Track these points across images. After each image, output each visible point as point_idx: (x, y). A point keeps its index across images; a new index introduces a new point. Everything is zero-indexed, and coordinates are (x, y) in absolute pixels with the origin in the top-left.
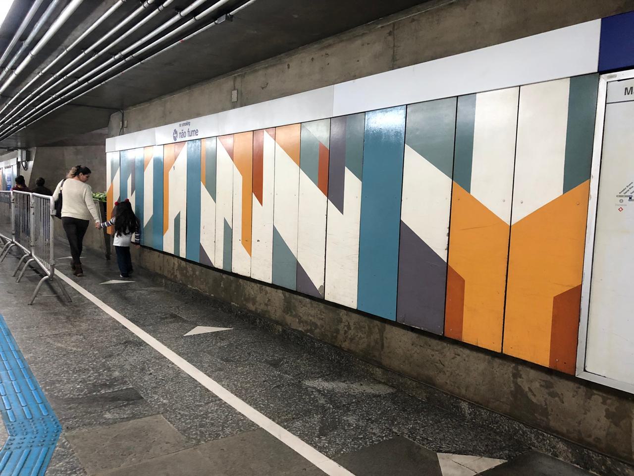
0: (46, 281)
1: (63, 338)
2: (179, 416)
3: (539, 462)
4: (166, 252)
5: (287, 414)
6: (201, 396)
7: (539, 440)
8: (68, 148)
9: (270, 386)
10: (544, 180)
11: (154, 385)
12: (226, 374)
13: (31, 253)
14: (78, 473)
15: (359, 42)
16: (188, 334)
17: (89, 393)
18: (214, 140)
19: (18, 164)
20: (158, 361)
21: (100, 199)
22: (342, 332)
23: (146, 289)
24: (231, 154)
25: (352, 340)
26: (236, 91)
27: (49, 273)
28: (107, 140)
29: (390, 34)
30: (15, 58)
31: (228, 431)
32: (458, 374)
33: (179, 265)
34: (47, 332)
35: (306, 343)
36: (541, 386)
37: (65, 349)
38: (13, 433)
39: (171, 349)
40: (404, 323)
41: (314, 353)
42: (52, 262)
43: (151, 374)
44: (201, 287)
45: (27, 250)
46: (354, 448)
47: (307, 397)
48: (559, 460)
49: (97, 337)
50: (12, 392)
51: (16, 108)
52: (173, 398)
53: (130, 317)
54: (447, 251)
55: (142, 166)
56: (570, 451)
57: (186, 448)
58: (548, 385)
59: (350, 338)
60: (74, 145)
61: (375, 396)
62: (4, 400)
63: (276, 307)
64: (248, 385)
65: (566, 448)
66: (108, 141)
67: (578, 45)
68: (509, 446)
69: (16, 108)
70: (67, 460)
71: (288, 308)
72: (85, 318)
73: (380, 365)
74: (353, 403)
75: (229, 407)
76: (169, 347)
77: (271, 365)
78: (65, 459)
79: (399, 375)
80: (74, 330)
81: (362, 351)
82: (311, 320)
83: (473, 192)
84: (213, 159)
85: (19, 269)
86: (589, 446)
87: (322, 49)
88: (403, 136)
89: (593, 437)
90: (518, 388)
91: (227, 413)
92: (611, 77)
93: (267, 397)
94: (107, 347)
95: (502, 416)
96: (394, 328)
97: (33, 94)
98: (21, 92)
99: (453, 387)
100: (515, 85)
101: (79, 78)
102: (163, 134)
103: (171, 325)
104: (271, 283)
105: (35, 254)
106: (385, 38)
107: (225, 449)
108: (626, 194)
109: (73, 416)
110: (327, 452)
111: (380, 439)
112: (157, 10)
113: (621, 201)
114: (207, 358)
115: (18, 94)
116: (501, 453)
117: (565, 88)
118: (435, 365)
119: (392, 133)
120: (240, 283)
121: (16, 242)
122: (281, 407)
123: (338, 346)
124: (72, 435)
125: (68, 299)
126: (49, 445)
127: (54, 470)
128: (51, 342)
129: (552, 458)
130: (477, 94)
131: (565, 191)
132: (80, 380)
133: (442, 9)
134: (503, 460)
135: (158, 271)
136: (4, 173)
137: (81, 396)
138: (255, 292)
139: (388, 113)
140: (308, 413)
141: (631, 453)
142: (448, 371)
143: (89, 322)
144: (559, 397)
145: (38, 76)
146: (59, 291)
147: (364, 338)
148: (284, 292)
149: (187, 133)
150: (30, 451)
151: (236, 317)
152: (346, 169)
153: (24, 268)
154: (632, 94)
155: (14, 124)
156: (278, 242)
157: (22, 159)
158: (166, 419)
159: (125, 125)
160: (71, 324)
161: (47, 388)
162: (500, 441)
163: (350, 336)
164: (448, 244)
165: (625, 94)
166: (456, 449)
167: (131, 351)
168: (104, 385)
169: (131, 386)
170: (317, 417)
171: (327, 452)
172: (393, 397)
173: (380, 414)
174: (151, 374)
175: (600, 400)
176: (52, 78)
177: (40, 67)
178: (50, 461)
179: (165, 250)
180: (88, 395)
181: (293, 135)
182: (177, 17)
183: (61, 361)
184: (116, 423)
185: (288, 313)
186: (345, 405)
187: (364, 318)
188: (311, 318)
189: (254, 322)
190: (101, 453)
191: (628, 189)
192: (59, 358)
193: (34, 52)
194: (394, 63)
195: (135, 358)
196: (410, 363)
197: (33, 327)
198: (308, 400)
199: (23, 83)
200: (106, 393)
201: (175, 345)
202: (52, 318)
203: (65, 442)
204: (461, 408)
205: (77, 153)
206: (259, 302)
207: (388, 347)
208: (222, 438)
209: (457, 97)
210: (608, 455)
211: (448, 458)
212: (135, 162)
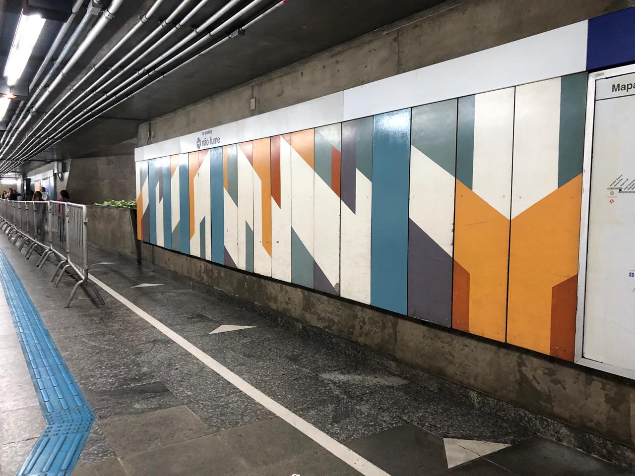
0: (81, 285)
1: (97, 338)
2: (202, 407)
3: (543, 447)
4: (193, 256)
5: (303, 404)
6: (223, 388)
7: (544, 426)
8: (101, 158)
9: (288, 380)
10: (539, 177)
11: (180, 379)
12: (247, 368)
13: (67, 260)
14: (109, 455)
15: (366, 48)
16: (210, 333)
17: (120, 386)
18: (235, 146)
19: (55, 175)
20: (183, 357)
21: (131, 206)
22: (358, 328)
23: (175, 291)
24: (251, 159)
25: (367, 334)
26: (254, 100)
27: (83, 277)
28: (135, 149)
29: (395, 40)
30: (48, 77)
31: (246, 419)
32: (467, 365)
33: (206, 267)
34: (83, 332)
35: (325, 339)
36: (545, 374)
37: (99, 347)
38: (51, 421)
39: (196, 346)
40: (414, 317)
41: (333, 348)
42: (86, 267)
43: (177, 369)
44: (227, 288)
45: (63, 257)
46: (364, 434)
47: (323, 389)
48: (563, 444)
49: (127, 336)
50: (50, 386)
51: (51, 122)
52: (197, 390)
53: (159, 317)
54: (452, 246)
55: (169, 174)
56: (572, 435)
57: (206, 434)
58: (550, 373)
59: (365, 333)
60: (107, 155)
61: (389, 387)
62: (43, 393)
63: (296, 305)
64: (268, 378)
65: (569, 433)
66: (136, 150)
67: (569, 44)
68: (515, 432)
69: (51, 122)
70: (99, 444)
71: (308, 306)
72: (117, 319)
73: (395, 359)
74: (367, 393)
75: (249, 398)
76: (194, 344)
77: (291, 359)
78: (98, 443)
79: (412, 367)
80: (107, 330)
81: (376, 345)
82: (328, 317)
83: (476, 189)
84: (234, 165)
85: (57, 275)
86: (591, 430)
87: (333, 56)
88: (409, 137)
89: (595, 422)
90: (523, 377)
91: (247, 404)
92: (599, 75)
93: (285, 389)
94: (136, 345)
95: (508, 403)
96: (406, 322)
97: (65, 109)
98: (54, 108)
99: (462, 377)
100: (557, 76)
101: (198, 26)
102: (187, 143)
103: (198, 325)
104: (370, 304)
105: (71, 261)
106: (391, 44)
107: (243, 435)
108: (617, 187)
109: (106, 406)
110: (338, 438)
111: (390, 426)
112: (175, 28)
113: (612, 193)
114: (231, 354)
115: (52, 110)
116: (506, 438)
117: (556, 88)
118: (446, 357)
119: (399, 135)
120: (262, 283)
121: (54, 250)
122: (298, 398)
123: (355, 341)
124: (104, 422)
125: (101, 302)
126: (83, 431)
127: (88, 454)
128: (86, 341)
129: (556, 443)
130: (476, 95)
131: (560, 186)
132: (111, 375)
133: (442, 15)
134: (507, 445)
135: (186, 274)
136: (41, 184)
137: (113, 389)
138: (277, 292)
139: (395, 115)
140: (323, 402)
141: (630, 436)
142: (457, 362)
143: (120, 323)
144: (562, 384)
145: (69, 93)
146: (93, 295)
147: (378, 332)
148: (303, 290)
149: (209, 141)
150: (66, 437)
151: (259, 316)
152: (357, 171)
153: (61, 273)
154: (619, 90)
155: (50, 137)
156: (296, 244)
157: (58, 171)
158: (190, 408)
159: (152, 135)
160: (105, 325)
161: (82, 382)
162: (507, 428)
163: (365, 331)
164: (453, 240)
165: (613, 91)
166: (462, 435)
167: (159, 348)
168: (133, 380)
169: (158, 380)
170: (331, 407)
171: (338, 438)
172: (405, 389)
173: (392, 404)
174: (177, 369)
175: (600, 385)
176: (83, 94)
177: (71, 84)
178: (84, 445)
179: (192, 254)
180: (119, 388)
181: (306, 141)
182: (193, 34)
183: (95, 358)
184: (143, 412)
185: (307, 311)
186: (358, 396)
187: (377, 314)
188: (328, 315)
189: (276, 320)
190: (130, 438)
191: (618, 181)
192: (93, 355)
193: (20, 129)
194: (400, 69)
195: (162, 355)
196: (422, 355)
197: (70, 328)
198: (323, 391)
199: (57, 99)
200: (135, 386)
201: (201, 342)
202: (86, 319)
203: (98, 429)
204: (471, 398)
205: (109, 163)
206: (280, 301)
207: (401, 340)
208: (241, 425)
209: (458, 98)
210: (609, 439)
211: (454, 443)
212: (162, 170)
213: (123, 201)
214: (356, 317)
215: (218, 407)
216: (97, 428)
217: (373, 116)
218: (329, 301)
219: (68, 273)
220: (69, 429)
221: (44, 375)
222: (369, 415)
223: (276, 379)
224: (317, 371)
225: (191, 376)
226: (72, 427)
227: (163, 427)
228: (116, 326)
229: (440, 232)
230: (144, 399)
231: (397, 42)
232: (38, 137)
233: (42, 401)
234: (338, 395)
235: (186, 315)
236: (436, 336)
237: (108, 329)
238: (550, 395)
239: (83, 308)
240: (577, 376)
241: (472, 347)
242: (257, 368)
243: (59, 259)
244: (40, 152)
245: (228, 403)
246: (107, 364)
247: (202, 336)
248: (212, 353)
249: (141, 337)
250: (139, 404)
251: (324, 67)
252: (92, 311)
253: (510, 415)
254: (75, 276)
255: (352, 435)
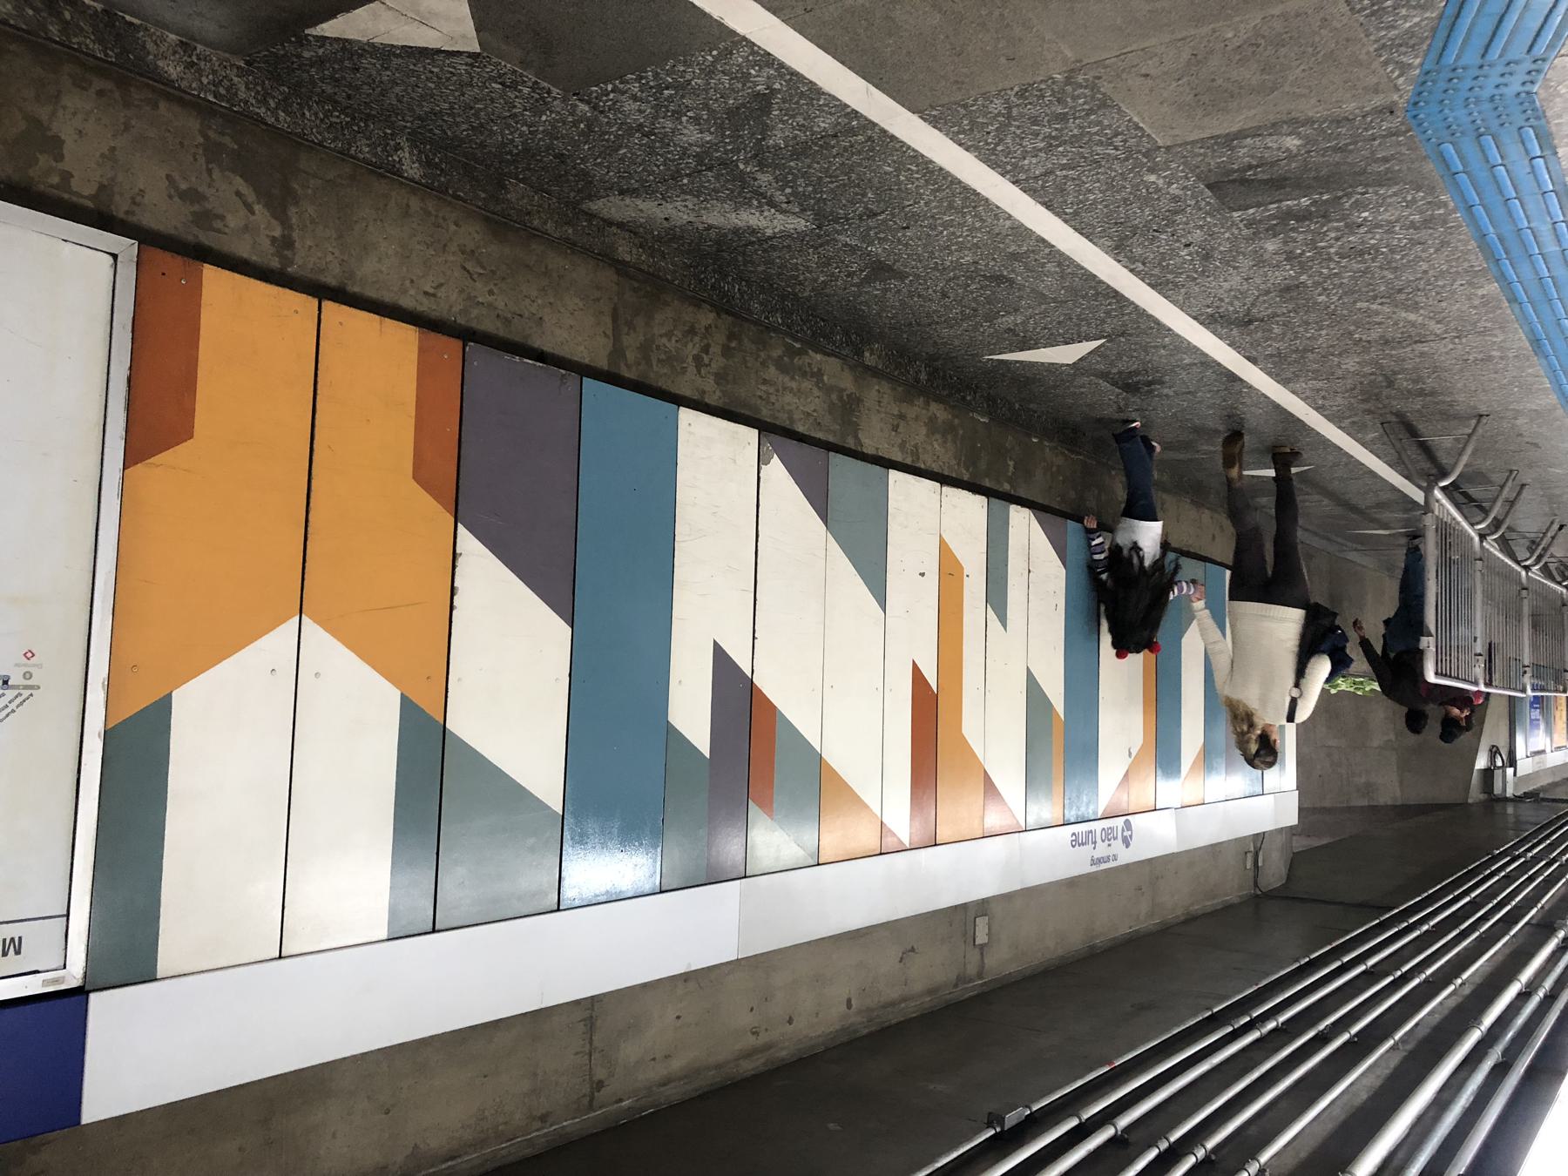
0: (1444, 474)
6: (1062, 190)
10: (222, 729)
15: (677, 1064)
18: (1031, 822)
19: (1512, 762)
20: (1170, 276)
22: (715, 349)
24: (990, 788)
25: (692, 331)
26: (978, 942)
28: (1295, 822)
29: (600, 1085)
30: (1520, 1021)
31: (997, 106)
34: (1442, 348)
36: (222, 218)
41: (783, 298)
42: (1429, 521)
53: (1237, 386)
58: (205, 218)
59: (695, 334)
60: (1374, 809)
61: (633, 192)
65: (160, 63)
67: (135, 1061)
70: (1394, 33)
71: (848, 408)
73: (620, 267)
77: (890, 269)
79: (575, 244)
82: (793, 378)
87: (768, 1047)
90: (279, 212)
95: (320, 144)
96: (587, 361)
98: (1507, 938)
102: (1158, 835)
106: (611, 1075)
107: (1003, 60)
108: (16, 692)
112: (1172, 1139)
113: (28, 675)
114: (1048, 284)
116: (321, 51)
117: (168, 956)
118: (483, 267)
122: (865, 163)
123: (724, 316)
128: (1432, 325)
132: (1362, 230)
137: (1360, 189)
140: (800, 151)
145: (1465, 976)
150: (1483, 56)
156: (873, 569)
160: (1381, 367)
162: (322, 80)
163: (697, 339)
164: (454, 567)
168: (1303, 216)
169: (1235, 214)
170: (777, 138)
171: (753, 53)
172: (589, 188)
173: (620, 147)
175: (75, 184)
176: (1429, 972)
178: (1434, 30)
181: (837, 834)
182: (1124, 1121)
183: (1408, 276)
184: (1274, 125)
187: (664, 384)
188: (794, 385)
191: (13, 706)
194: (589, 1011)
199: (1500, 958)
200: (1298, 198)
202: (1430, 383)
205: (1369, 789)
206: (920, 423)
212: (761, 805)
213: (1333, 691)
214: (720, 377)
215: (1074, 140)
216: (1401, 80)
217: (661, 892)
218: (791, 419)
219: (1481, 508)
220: (1476, 78)
221: (1545, 229)
222: (677, 115)
223: (926, 218)
224: (819, 237)
225: (1147, 225)
226: (1468, 83)
227: (1219, 82)
228: (1350, 364)
229: (490, 590)
230: (1273, 164)
231: (595, 1079)
232: (1554, 860)
233: (1551, 159)
234: (761, 170)
235: (1166, 391)
236: (507, 322)
237: (1373, 355)
238: (208, 162)
239: (1442, 413)
240: (135, 208)
241: (412, 292)
242: (976, 246)
243: (1504, 544)
244: (1551, 823)
245: (1049, 149)
246: (1373, 260)
247: (1122, 335)
248: (1094, 288)
249: (1284, 334)
250: (1288, 150)
251: (790, 1021)
252: (1417, 404)
253: (316, 114)
254: (1461, 499)
255: (716, 59)
